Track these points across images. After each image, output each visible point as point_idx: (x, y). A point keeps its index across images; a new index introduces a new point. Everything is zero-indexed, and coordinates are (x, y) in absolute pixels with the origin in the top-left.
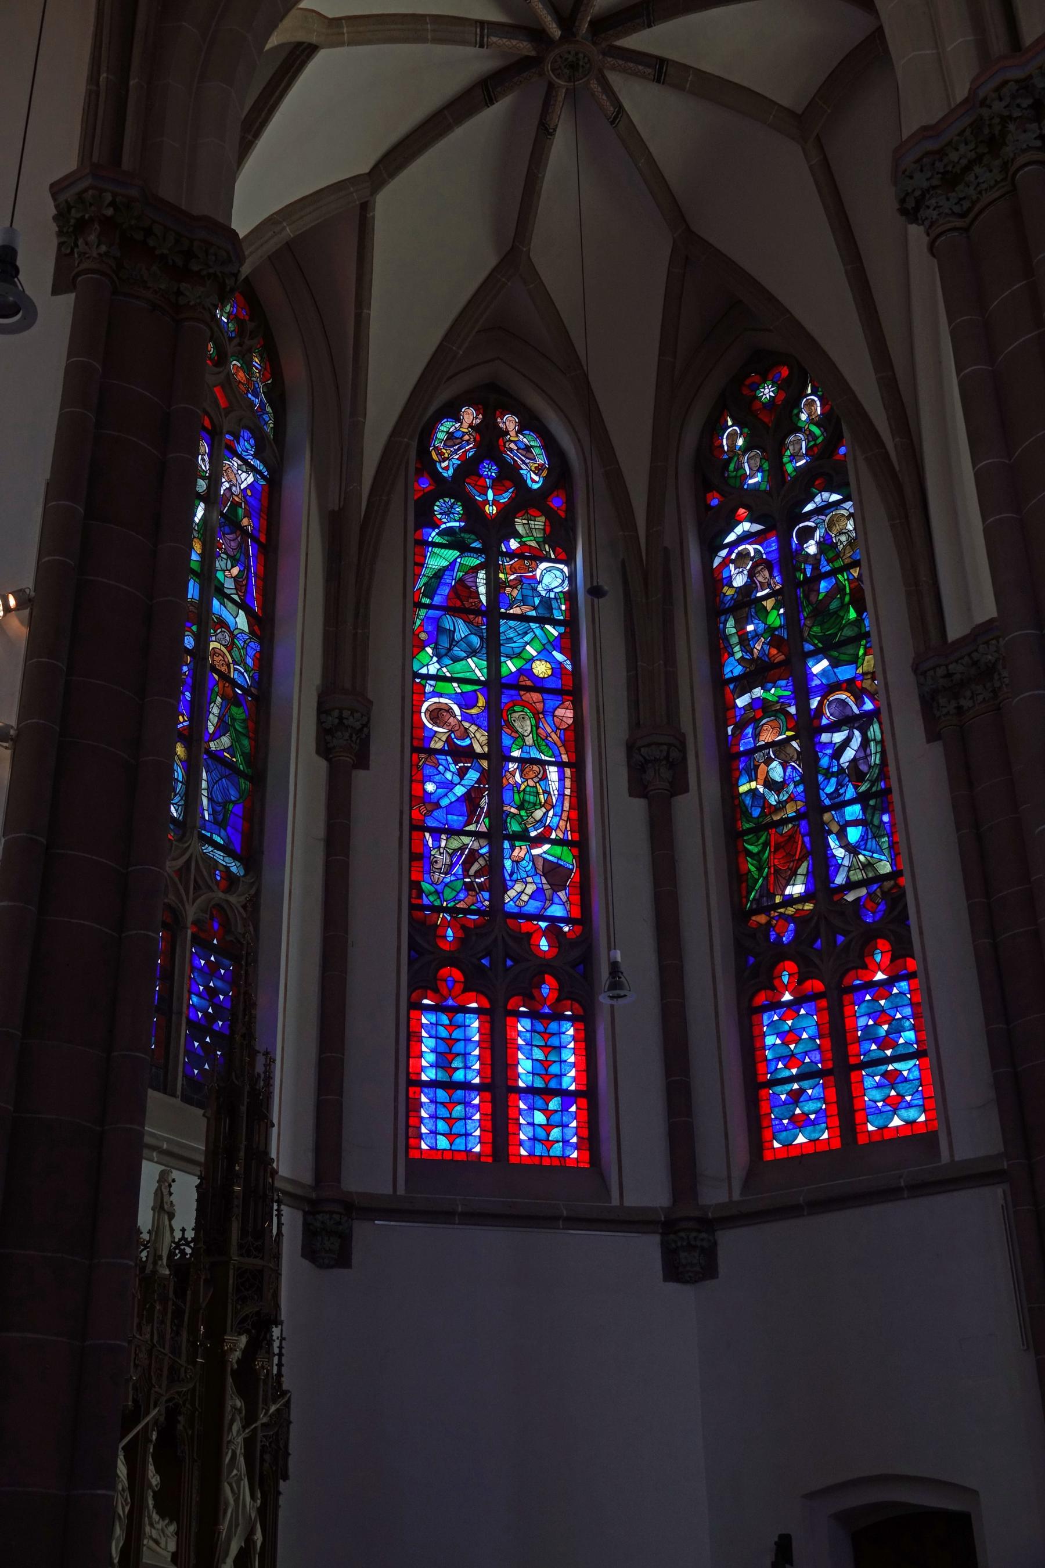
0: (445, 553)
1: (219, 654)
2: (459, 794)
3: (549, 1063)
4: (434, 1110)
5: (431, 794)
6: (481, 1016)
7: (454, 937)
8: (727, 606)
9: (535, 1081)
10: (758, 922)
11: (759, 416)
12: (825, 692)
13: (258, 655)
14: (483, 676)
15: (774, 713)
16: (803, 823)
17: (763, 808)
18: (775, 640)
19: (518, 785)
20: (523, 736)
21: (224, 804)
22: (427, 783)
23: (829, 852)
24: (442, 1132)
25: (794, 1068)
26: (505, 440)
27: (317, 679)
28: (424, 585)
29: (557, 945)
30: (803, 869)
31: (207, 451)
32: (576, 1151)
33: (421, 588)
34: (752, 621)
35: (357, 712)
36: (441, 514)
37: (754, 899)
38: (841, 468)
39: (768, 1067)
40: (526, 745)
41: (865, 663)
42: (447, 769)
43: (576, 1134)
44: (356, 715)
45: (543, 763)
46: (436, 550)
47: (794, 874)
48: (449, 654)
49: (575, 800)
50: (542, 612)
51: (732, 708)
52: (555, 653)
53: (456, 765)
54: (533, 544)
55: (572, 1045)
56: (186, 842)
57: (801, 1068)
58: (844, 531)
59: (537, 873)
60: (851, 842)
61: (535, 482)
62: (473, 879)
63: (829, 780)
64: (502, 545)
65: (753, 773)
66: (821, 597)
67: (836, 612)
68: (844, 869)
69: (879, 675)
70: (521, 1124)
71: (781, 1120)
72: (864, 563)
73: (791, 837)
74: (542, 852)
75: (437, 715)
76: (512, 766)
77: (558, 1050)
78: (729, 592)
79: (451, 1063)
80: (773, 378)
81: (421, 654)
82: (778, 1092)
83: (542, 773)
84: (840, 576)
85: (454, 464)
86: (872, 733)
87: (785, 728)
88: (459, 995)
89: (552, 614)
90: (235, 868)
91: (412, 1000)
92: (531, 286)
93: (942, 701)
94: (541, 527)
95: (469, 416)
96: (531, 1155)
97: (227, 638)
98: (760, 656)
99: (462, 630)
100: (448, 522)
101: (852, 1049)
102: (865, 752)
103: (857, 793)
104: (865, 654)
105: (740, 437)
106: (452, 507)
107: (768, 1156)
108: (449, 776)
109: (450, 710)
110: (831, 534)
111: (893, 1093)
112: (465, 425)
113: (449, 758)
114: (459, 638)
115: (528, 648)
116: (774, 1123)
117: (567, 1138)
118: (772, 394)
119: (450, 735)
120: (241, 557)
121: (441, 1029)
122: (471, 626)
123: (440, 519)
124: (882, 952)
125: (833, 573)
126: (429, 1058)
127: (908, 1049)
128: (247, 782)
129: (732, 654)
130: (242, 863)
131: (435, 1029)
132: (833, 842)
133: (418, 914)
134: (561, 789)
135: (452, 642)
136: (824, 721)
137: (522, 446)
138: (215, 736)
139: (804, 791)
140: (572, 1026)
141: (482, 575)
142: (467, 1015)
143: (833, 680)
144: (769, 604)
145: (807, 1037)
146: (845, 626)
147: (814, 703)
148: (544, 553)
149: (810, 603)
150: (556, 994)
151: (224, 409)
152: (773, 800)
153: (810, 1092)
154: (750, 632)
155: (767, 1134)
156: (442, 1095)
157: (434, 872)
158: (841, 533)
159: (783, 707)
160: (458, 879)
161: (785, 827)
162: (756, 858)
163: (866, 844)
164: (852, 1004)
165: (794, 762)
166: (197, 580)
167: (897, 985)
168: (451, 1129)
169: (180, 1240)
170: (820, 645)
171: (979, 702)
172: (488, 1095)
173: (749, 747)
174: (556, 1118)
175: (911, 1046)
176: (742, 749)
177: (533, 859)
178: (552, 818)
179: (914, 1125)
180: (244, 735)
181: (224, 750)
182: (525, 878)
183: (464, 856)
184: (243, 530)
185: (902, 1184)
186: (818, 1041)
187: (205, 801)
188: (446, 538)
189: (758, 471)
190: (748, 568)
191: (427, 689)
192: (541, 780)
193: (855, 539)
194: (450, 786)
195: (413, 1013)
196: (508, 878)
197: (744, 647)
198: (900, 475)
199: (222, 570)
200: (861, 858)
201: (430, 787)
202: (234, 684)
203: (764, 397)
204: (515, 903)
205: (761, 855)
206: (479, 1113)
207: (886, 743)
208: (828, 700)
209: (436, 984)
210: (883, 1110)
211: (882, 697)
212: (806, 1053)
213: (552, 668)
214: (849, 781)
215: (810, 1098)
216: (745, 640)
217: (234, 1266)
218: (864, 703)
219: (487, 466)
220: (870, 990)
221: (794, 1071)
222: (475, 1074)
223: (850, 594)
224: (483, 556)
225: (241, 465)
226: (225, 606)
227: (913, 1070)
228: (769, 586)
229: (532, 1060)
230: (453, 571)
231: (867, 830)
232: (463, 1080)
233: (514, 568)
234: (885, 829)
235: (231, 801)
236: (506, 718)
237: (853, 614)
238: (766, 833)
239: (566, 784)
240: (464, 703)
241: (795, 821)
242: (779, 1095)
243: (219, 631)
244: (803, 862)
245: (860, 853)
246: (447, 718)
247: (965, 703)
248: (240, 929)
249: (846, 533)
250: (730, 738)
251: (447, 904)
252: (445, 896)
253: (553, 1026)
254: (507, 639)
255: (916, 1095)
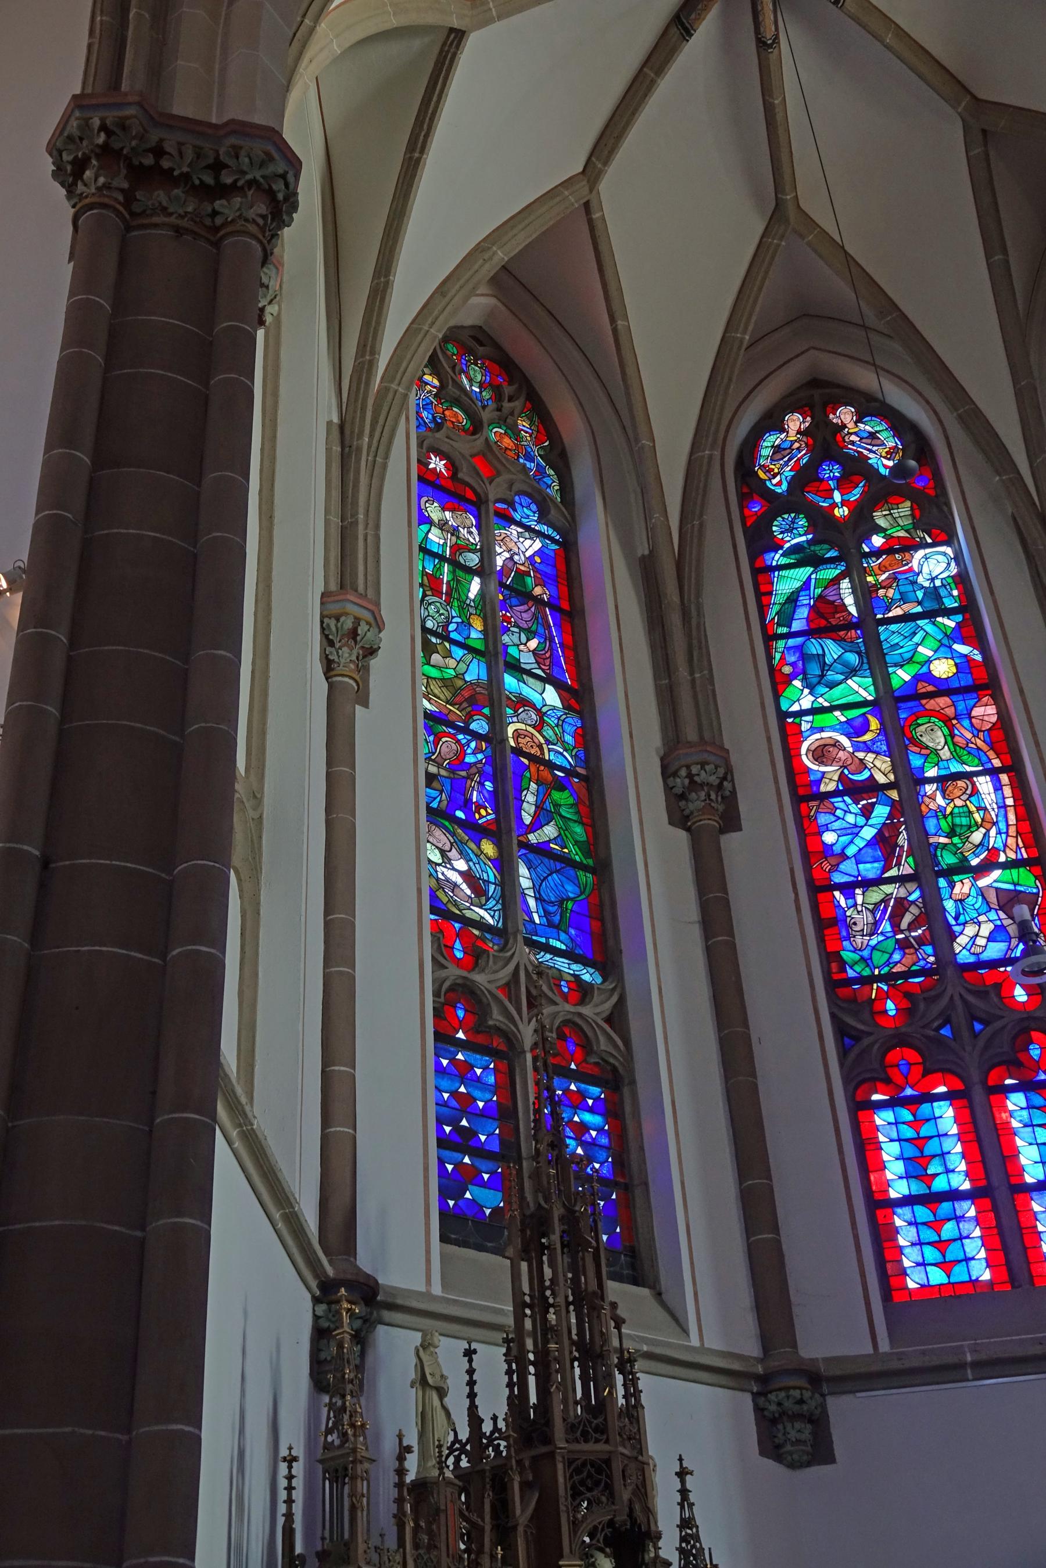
1: (525, 736)
4: (916, 1235)
7: (897, 1009)
20: (936, 750)
21: (561, 902)
31: (474, 523)
33: (774, 618)
35: (708, 764)
36: (782, 533)
40: (942, 760)
44: (707, 767)
45: (969, 776)
46: (783, 573)
49: (1022, 810)
50: (930, 605)
53: (856, 803)
54: (902, 534)
56: (511, 949)
61: (883, 465)
62: (907, 933)
70: (1040, 1233)
75: (821, 754)
76: (929, 789)
79: (926, 1170)
88: (920, 1080)
89: (943, 603)
91: (858, 1099)
92: (810, 238)
94: (907, 513)
95: (795, 422)
97: (534, 716)
99: (832, 650)
106: (793, 522)
108: (851, 819)
109: (836, 744)
113: (846, 798)
119: (842, 772)
122: (843, 644)
123: (782, 539)
126: (894, 1169)
128: (588, 875)
130: (597, 969)
133: (842, 992)
134: (1000, 801)
135: (824, 667)
137: (866, 435)
138: (536, 825)
141: (845, 584)
148: (918, 540)
156: (923, 1213)
157: (854, 937)
160: (888, 938)
166: (481, 659)
169: (492, 1433)
177: (981, 892)
180: (575, 821)
184: (538, 601)
188: (793, 557)
192: (971, 796)
194: (856, 830)
199: (514, 645)
201: (829, 838)
202: (551, 766)
209: (886, 1073)
213: (956, 665)
217: (563, 1458)
219: (827, 468)
226: (525, 683)
229: (1037, 1144)
230: (809, 589)
232: (947, 1188)
233: (884, 566)
235: (569, 899)
239: (1005, 793)
243: (521, 710)
246: (835, 753)
248: (603, 1045)
251: (879, 972)
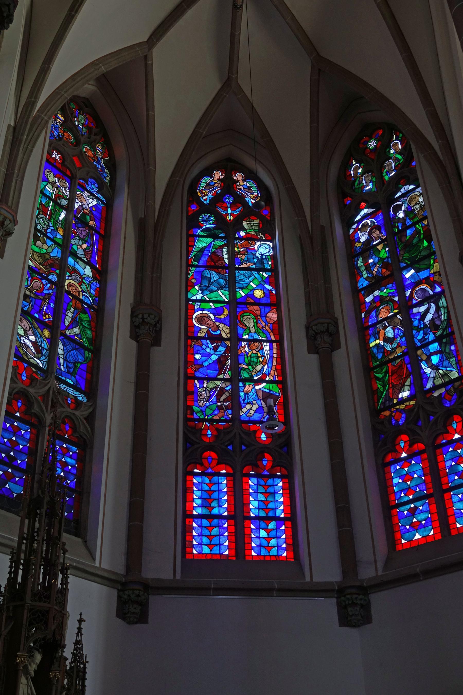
0: (205, 240)
1: (73, 286)
2: (214, 360)
3: (268, 502)
4: (201, 531)
5: (198, 360)
6: (228, 478)
7: (212, 435)
8: (358, 252)
13: (98, 289)
15: (387, 302)
16: (406, 358)
17: (384, 353)
18: (384, 264)
19: (247, 353)
20: (249, 328)
22: (196, 355)
24: (206, 544)
25: (410, 495)
26: (237, 185)
27: (131, 300)
28: (194, 256)
30: (408, 382)
31: (68, 186)
32: (285, 552)
33: (192, 257)
35: (152, 315)
36: (203, 221)
38: (413, 171)
39: (395, 496)
40: (251, 333)
41: (435, 268)
42: (207, 347)
43: (285, 542)
44: (151, 316)
45: (261, 341)
46: (200, 239)
47: (403, 386)
48: (208, 289)
49: (279, 360)
50: (259, 266)
51: (363, 304)
52: (266, 286)
53: (212, 344)
54: (253, 233)
55: (281, 492)
56: (48, 380)
57: (414, 495)
58: (418, 202)
59: (259, 399)
60: (434, 364)
61: (251, 202)
62: (222, 403)
63: (419, 332)
64: (236, 234)
65: (377, 335)
66: (408, 238)
67: (416, 244)
69: (443, 273)
71: (405, 526)
72: (429, 217)
73: (400, 366)
74: (261, 387)
75: (201, 320)
76: (243, 344)
77: (273, 494)
78: (358, 245)
79: (210, 505)
80: (375, 136)
81: (192, 289)
82: (402, 510)
83: (260, 346)
84: (417, 226)
85: (210, 197)
86: (442, 303)
89: (264, 266)
90: (80, 398)
92: (239, 96)
94: (257, 225)
95: (218, 175)
96: (259, 555)
97: (79, 278)
99: (215, 276)
101: (444, 480)
102: (438, 314)
103: (435, 337)
104: (434, 263)
105: (360, 168)
106: (209, 218)
107: (399, 548)
108: (208, 350)
109: (208, 317)
110: (411, 205)
112: (216, 179)
113: (208, 341)
114: (213, 281)
115: (251, 284)
116: (401, 529)
117: (280, 545)
118: (375, 144)
119: (208, 330)
120: (89, 240)
121: (204, 485)
122: (219, 275)
123: (203, 224)
124: (457, 423)
125: (414, 225)
128: (90, 353)
129: (362, 276)
131: (201, 485)
136: (414, 302)
137: (246, 187)
138: (71, 327)
139: (406, 340)
140: (281, 481)
141: (225, 249)
142: (220, 477)
143: (417, 279)
144: (380, 247)
147: (408, 293)
149: (402, 242)
150: (271, 464)
151: (78, 167)
152: (389, 348)
153: (421, 508)
154: (371, 263)
155: (398, 535)
156: (205, 522)
157: (200, 401)
158: (416, 204)
159: (391, 298)
161: (396, 362)
162: (382, 380)
163: (443, 363)
164: (442, 454)
165: (399, 326)
166: (60, 248)
168: (211, 542)
170: (409, 263)
172: (232, 522)
173: (374, 322)
174: (273, 533)
176: (370, 324)
177: (256, 391)
180: (88, 329)
181: (75, 335)
182: (252, 402)
183: (217, 391)
184: (90, 227)
186: (423, 478)
187: (62, 361)
188: (206, 232)
189: (370, 183)
190: (368, 231)
191: (196, 307)
192: (260, 350)
193: (424, 206)
194: (209, 355)
195: (188, 478)
196: (242, 402)
197: (368, 271)
201: (198, 356)
202: (82, 302)
203: (371, 146)
204: (246, 415)
205: (384, 379)
206: (227, 532)
207: (449, 308)
208: (415, 290)
211: (445, 284)
212: (417, 486)
214: (430, 331)
215: (421, 512)
216: (368, 268)
217: (28, 607)
218: (435, 288)
219: (227, 198)
221: (411, 497)
222: (225, 510)
223: (424, 233)
225: (89, 195)
228: (379, 238)
229: (258, 501)
231: (442, 356)
234: (453, 353)
235: (79, 362)
236: (239, 319)
237: (426, 244)
238: (386, 366)
239: (274, 351)
243: (73, 274)
244: (408, 379)
249: (419, 203)
251: (207, 417)
252: (207, 413)
253: (270, 481)
254: (240, 280)
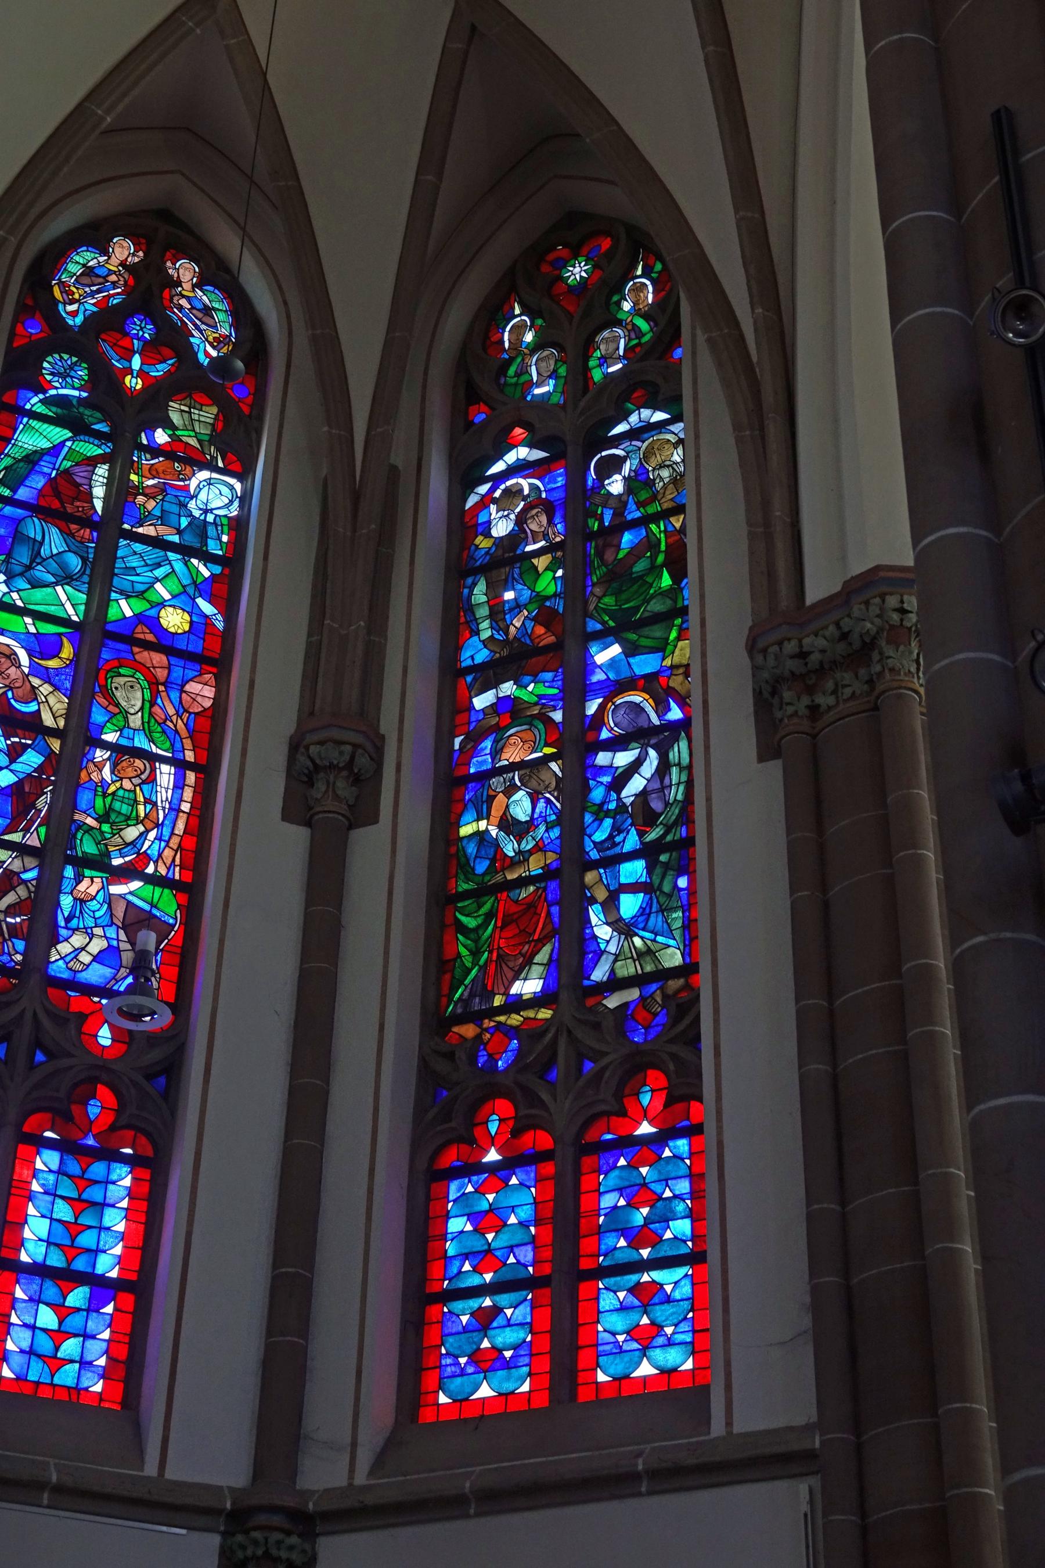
0: (49, 430)
3: (80, 1228)
8: (478, 563)
9: (50, 1255)
10: (461, 1036)
11: (561, 303)
12: (611, 692)
14: (77, 615)
15: (529, 719)
16: (553, 885)
17: (493, 860)
18: (546, 616)
20: (127, 712)
23: (587, 931)
26: (174, 293)
29: (127, 1040)
30: (543, 955)
32: (101, 1381)
34: (513, 585)
36: (52, 374)
37: (460, 999)
40: (129, 727)
41: (677, 651)
45: (152, 758)
46: (34, 423)
47: (529, 962)
48: (27, 574)
49: (195, 821)
50: (190, 540)
52: (200, 601)
54: (193, 442)
55: (124, 1204)
58: (668, 463)
60: (624, 917)
61: (206, 352)
63: (601, 821)
64: (143, 435)
65: (485, 806)
66: (621, 555)
68: (607, 959)
71: (456, 1357)
72: (691, 509)
73: (530, 906)
74: (127, 891)
76: (100, 754)
77: (99, 1208)
80: (588, 253)
82: (456, 1311)
84: (653, 527)
86: (677, 754)
87: (542, 742)
89: (206, 545)
93: (787, 695)
94: (208, 420)
95: (123, 250)
98: (519, 636)
99: (55, 542)
100: (62, 388)
101: (586, 1245)
102: (662, 782)
103: (641, 843)
104: (679, 638)
105: (530, 330)
106: (71, 367)
109: (12, 657)
110: (647, 466)
111: (645, 1320)
112: (115, 261)
114: (48, 554)
115: (158, 586)
116: (443, 1362)
118: (584, 274)
123: (50, 382)
124: (652, 1091)
127: (678, 1248)
129: (477, 633)
132: (595, 915)
134: (175, 801)
135: (36, 557)
136: (605, 734)
141: (102, 470)
143: (626, 673)
144: (541, 563)
145: (516, 1222)
146: (653, 597)
150: (110, 1118)
153: (509, 1312)
154: (508, 601)
158: (662, 466)
159: (543, 711)
161: (523, 890)
162: (472, 936)
163: (647, 920)
165: (549, 793)
167: (671, 1144)
170: (612, 624)
171: (845, 697)
173: (484, 768)
175: (683, 1244)
176: (472, 771)
177: (110, 900)
178: (153, 842)
179: (673, 1375)
182: (91, 928)
185: (640, 1467)
186: (532, 1229)
188: (54, 409)
189: (550, 377)
190: (518, 510)
192: (144, 782)
196: (62, 923)
197: (496, 622)
198: (757, 370)
200: (637, 941)
203: (572, 277)
204: (67, 964)
207: (695, 771)
208: (613, 704)
210: (625, 1347)
212: (511, 1249)
213: (191, 623)
214: (631, 825)
216: (498, 613)
220: (627, 1150)
221: (488, 1277)
223: (666, 552)
224: (109, 445)
227: (683, 1283)
228: (545, 536)
229: (51, 1219)
230: (57, 458)
231: (651, 899)
236: (102, 683)
237: (666, 581)
238: (493, 898)
239: (185, 794)
240: (38, 649)
241: (540, 882)
242: (458, 1316)
244: (544, 945)
245: (637, 935)
247: (824, 700)
249: (671, 465)
250: (456, 755)
253: (97, 1169)
255: (682, 1325)
